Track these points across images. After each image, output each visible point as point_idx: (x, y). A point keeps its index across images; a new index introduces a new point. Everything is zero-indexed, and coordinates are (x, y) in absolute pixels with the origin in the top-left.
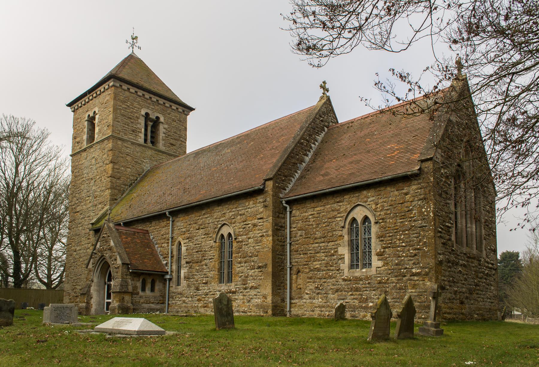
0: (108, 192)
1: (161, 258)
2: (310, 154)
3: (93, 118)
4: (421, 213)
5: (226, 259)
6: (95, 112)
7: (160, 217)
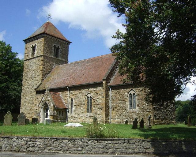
5: (90, 105)
6: (35, 45)
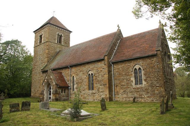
0: (46, 59)
1: (67, 81)
2: (117, 47)
3: (42, 36)
4: (158, 67)
7: (66, 68)
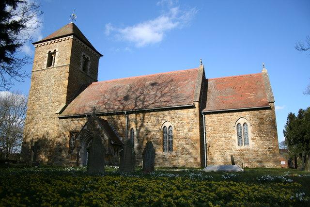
6: (55, 51)
